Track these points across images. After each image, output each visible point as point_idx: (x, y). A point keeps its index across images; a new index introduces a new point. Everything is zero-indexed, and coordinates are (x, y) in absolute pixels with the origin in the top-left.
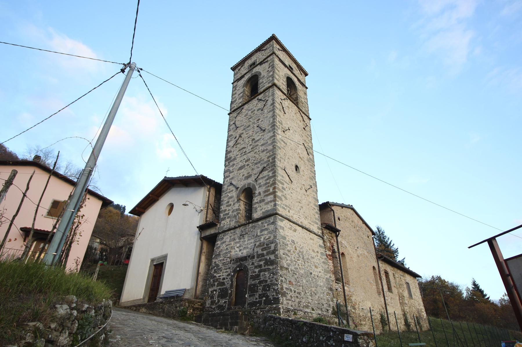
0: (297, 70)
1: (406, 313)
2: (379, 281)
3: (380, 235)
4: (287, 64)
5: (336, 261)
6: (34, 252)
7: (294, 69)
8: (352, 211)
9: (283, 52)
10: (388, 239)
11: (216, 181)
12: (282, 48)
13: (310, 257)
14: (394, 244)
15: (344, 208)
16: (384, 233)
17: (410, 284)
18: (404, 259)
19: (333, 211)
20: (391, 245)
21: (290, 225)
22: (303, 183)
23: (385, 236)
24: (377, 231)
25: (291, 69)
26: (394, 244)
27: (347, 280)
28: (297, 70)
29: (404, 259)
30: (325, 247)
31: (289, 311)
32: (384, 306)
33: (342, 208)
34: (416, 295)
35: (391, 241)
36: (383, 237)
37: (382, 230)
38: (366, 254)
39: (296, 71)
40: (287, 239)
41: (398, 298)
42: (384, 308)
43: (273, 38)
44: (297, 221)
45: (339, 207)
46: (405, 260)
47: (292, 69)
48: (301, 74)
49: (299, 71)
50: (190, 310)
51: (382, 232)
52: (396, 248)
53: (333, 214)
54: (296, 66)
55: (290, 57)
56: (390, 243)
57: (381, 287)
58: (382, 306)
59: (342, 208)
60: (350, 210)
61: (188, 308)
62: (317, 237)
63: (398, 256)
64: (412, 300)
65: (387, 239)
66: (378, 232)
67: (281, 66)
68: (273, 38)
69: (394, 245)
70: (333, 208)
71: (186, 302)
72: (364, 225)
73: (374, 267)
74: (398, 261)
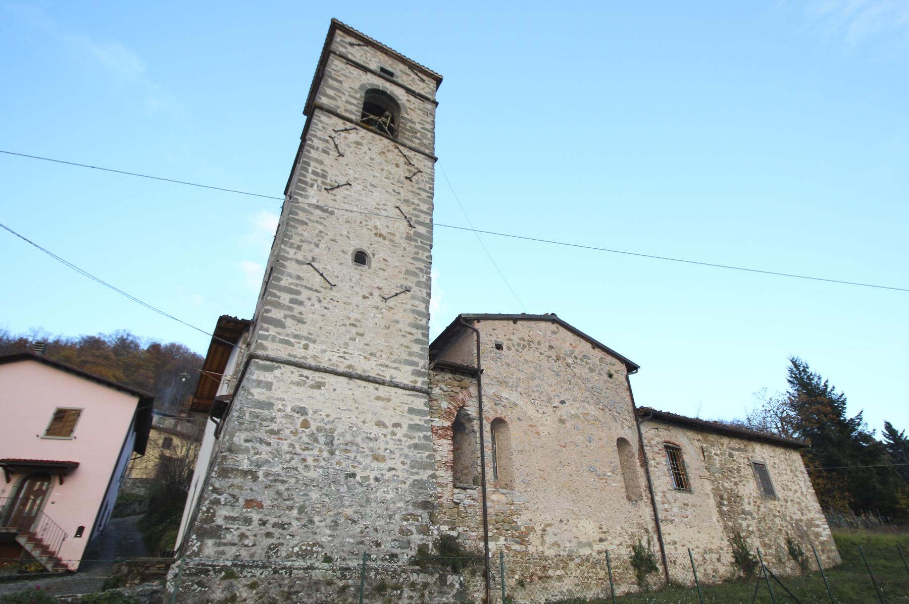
0: (405, 73)
1: (743, 534)
2: (640, 471)
3: (800, 374)
4: (373, 66)
5: (474, 439)
6: (26, 498)
7: (397, 72)
8: (553, 327)
9: (366, 48)
10: (819, 378)
11: (240, 318)
12: (363, 41)
13: (358, 440)
14: (834, 387)
15: (519, 322)
16: (807, 367)
17: (769, 468)
18: (861, 413)
19: (477, 331)
20: (829, 390)
21: (301, 376)
22: (376, 285)
23: (811, 374)
24: (793, 366)
25: (386, 76)
26: (834, 387)
27: (510, 478)
28: (405, 73)
29: (861, 413)
30: (431, 412)
31: (208, 571)
32: (651, 526)
33: (515, 323)
34: (791, 490)
35: (827, 381)
36: (808, 377)
37: (804, 364)
38: (598, 413)
39: (405, 77)
40: (278, 405)
41: (712, 502)
42: (650, 529)
43: (335, 26)
44: (333, 365)
45: (505, 323)
46: (863, 415)
47: (392, 74)
48: (423, 81)
49: (413, 76)
50: (134, 579)
51: (804, 367)
52: (840, 394)
53: (475, 338)
54: (407, 68)
55: (386, 54)
56: (826, 386)
57: (643, 482)
58: (640, 526)
59: (515, 323)
60: (549, 324)
61: (127, 576)
62: (407, 392)
63: (845, 408)
64: (776, 503)
65: (816, 379)
66: (795, 369)
67: (352, 71)
68: (335, 26)
69: (835, 389)
70: (477, 326)
71: (122, 565)
72: (598, 353)
73: (622, 442)
74: (848, 418)
